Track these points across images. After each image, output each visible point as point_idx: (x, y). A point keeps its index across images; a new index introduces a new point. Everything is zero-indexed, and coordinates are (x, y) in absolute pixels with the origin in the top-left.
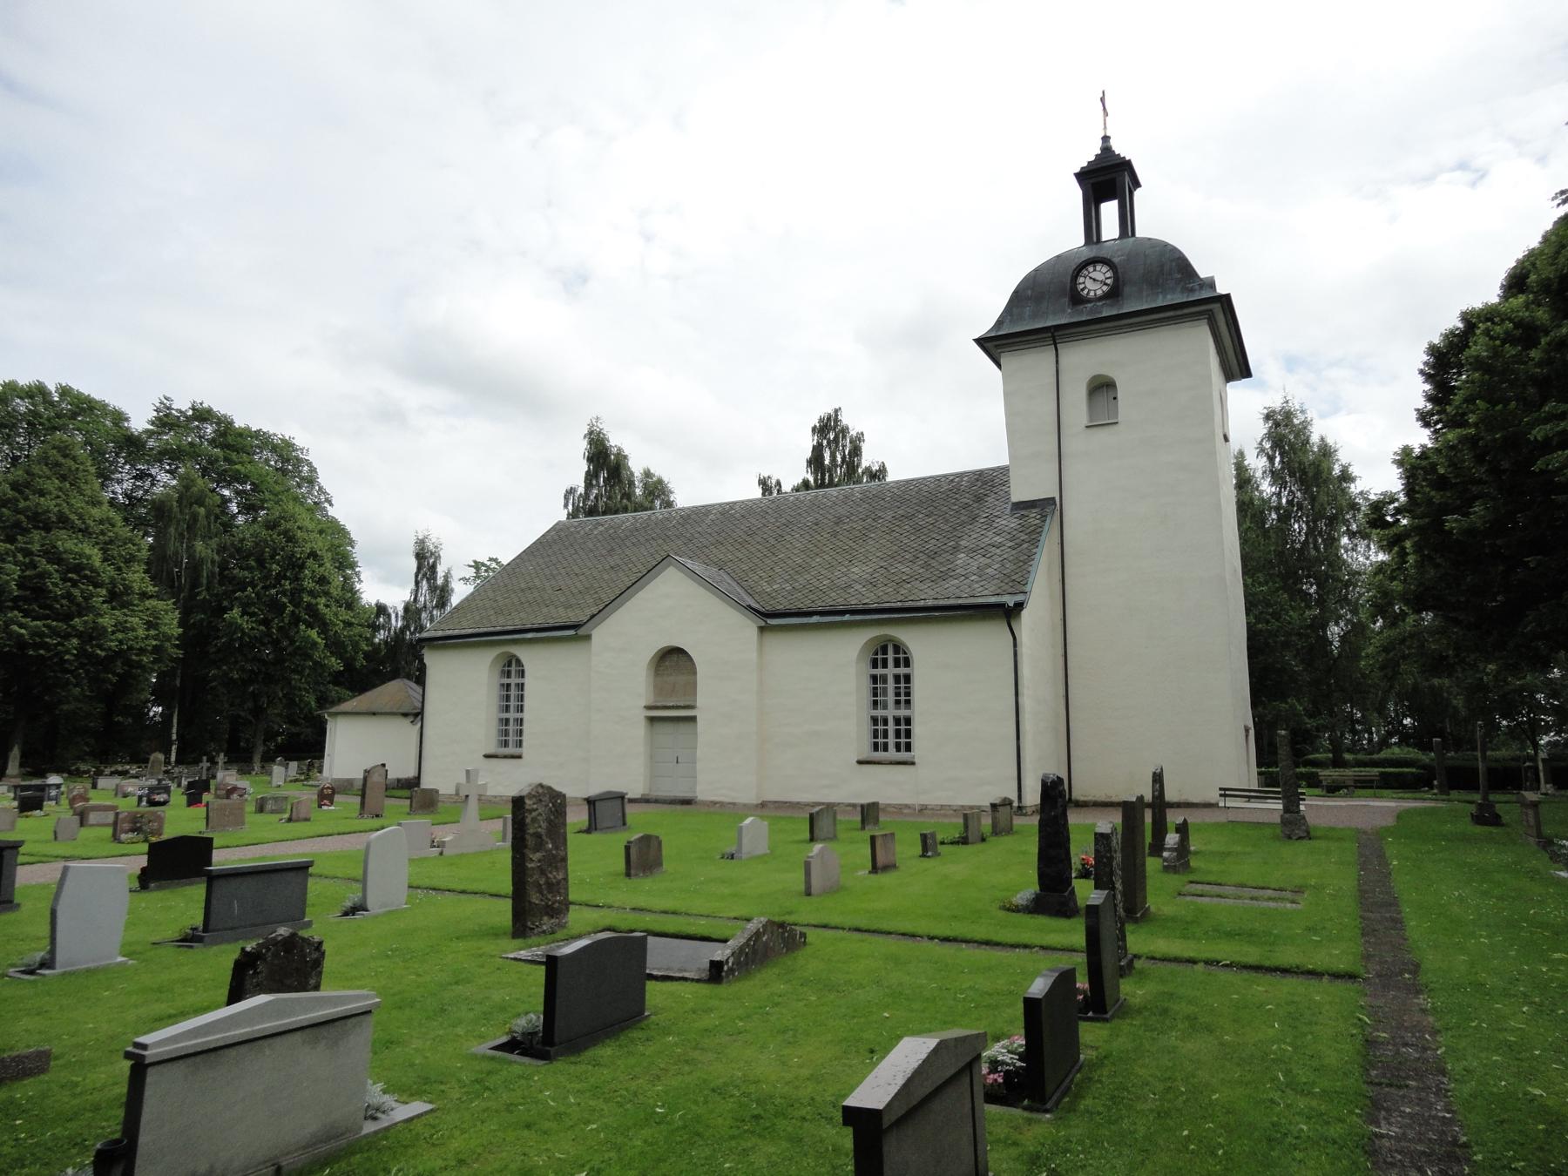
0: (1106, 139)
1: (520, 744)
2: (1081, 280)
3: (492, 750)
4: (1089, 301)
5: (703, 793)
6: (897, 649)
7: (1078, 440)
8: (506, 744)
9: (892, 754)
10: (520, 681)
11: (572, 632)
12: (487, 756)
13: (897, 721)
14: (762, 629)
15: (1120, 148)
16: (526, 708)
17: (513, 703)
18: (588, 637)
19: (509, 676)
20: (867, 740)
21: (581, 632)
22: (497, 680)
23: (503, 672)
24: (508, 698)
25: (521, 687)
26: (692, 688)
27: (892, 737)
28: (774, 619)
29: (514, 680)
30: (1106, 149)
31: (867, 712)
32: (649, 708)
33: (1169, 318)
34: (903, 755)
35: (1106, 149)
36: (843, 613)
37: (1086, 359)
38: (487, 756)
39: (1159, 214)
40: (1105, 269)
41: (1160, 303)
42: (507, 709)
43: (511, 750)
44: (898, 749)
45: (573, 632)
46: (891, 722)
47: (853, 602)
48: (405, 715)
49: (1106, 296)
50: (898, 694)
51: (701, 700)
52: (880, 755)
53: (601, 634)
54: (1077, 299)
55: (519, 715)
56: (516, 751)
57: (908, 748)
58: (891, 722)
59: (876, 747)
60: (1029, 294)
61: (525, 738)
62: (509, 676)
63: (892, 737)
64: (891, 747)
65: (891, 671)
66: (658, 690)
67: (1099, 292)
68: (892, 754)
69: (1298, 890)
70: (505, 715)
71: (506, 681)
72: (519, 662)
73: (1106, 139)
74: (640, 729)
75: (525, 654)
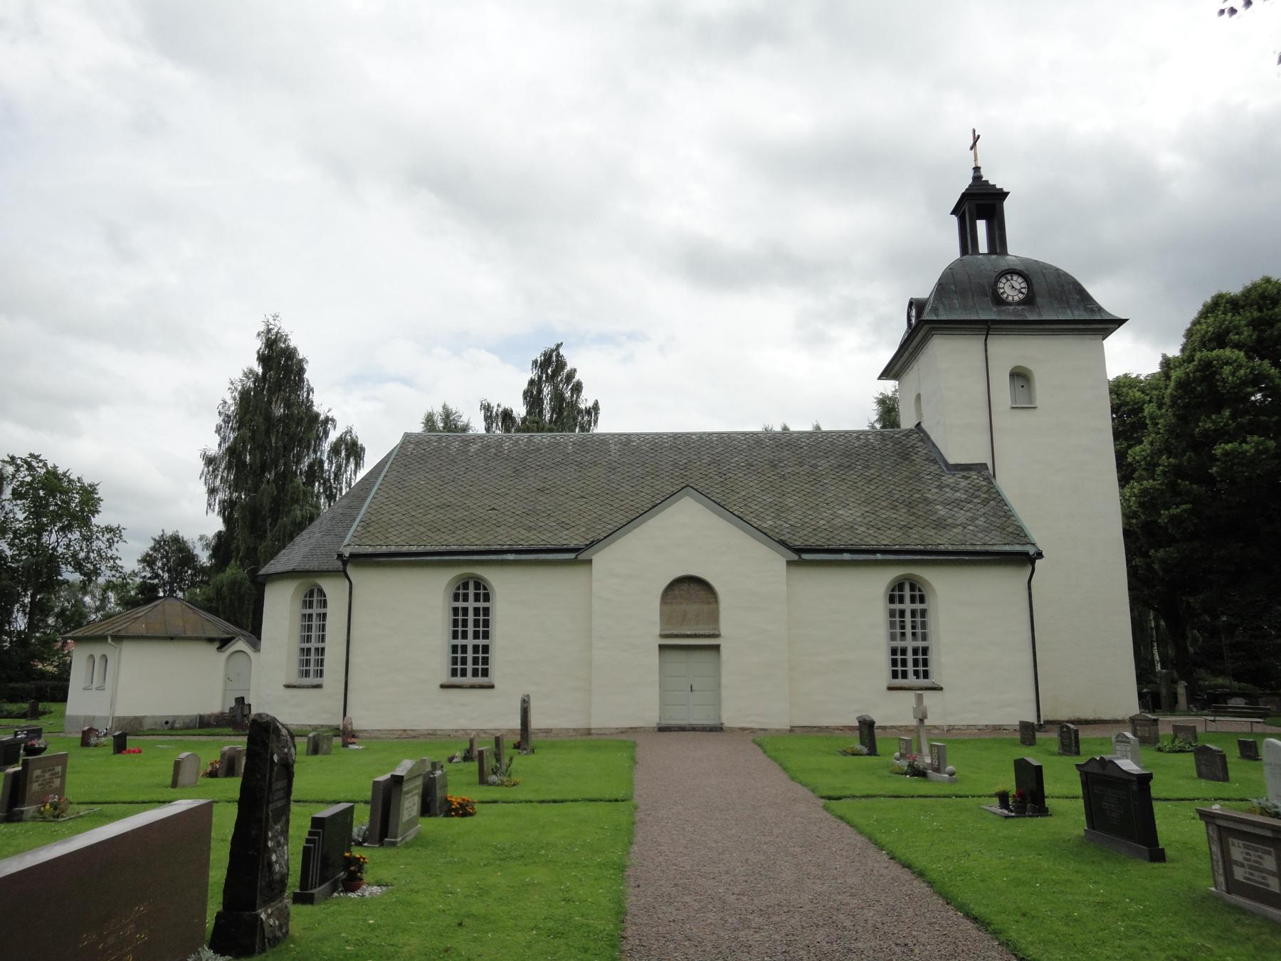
0: (977, 169)
1: (321, 674)
2: (1004, 280)
3: (295, 679)
4: (1009, 304)
5: (729, 720)
6: (913, 588)
7: (1005, 418)
8: (307, 674)
9: (470, 679)
10: (322, 611)
11: (572, 556)
12: (287, 686)
13: (915, 651)
14: (789, 563)
15: (995, 177)
16: (327, 639)
17: (314, 633)
18: (589, 562)
19: (311, 607)
20: (295, 667)
21: (582, 556)
22: (298, 610)
23: (305, 602)
24: (309, 628)
25: (323, 616)
26: (714, 618)
27: (910, 665)
28: (805, 555)
29: (315, 611)
30: (977, 178)
31: (296, 645)
32: (663, 636)
33: (1083, 330)
34: (480, 680)
35: (977, 178)
36: (874, 552)
37: (1010, 351)
38: (287, 686)
39: (1026, 238)
40: (1020, 280)
41: (1069, 317)
42: (309, 639)
43: (312, 680)
44: (916, 673)
45: (574, 556)
46: (910, 652)
47: (855, 541)
48: (211, 640)
49: (1020, 303)
50: (913, 627)
51: (725, 627)
52: (459, 680)
53: (602, 559)
54: (999, 301)
55: (320, 645)
56: (317, 681)
57: (485, 673)
58: (910, 652)
59: (454, 673)
60: (290, 354)
61: (325, 668)
62: (311, 607)
63: (910, 665)
64: (469, 672)
65: (908, 606)
66: (666, 618)
67: (1016, 298)
68: (911, 680)
69: (498, 760)
70: (306, 645)
71: (308, 611)
72: (321, 592)
73: (977, 169)
74: (653, 658)
75: (497, 579)
